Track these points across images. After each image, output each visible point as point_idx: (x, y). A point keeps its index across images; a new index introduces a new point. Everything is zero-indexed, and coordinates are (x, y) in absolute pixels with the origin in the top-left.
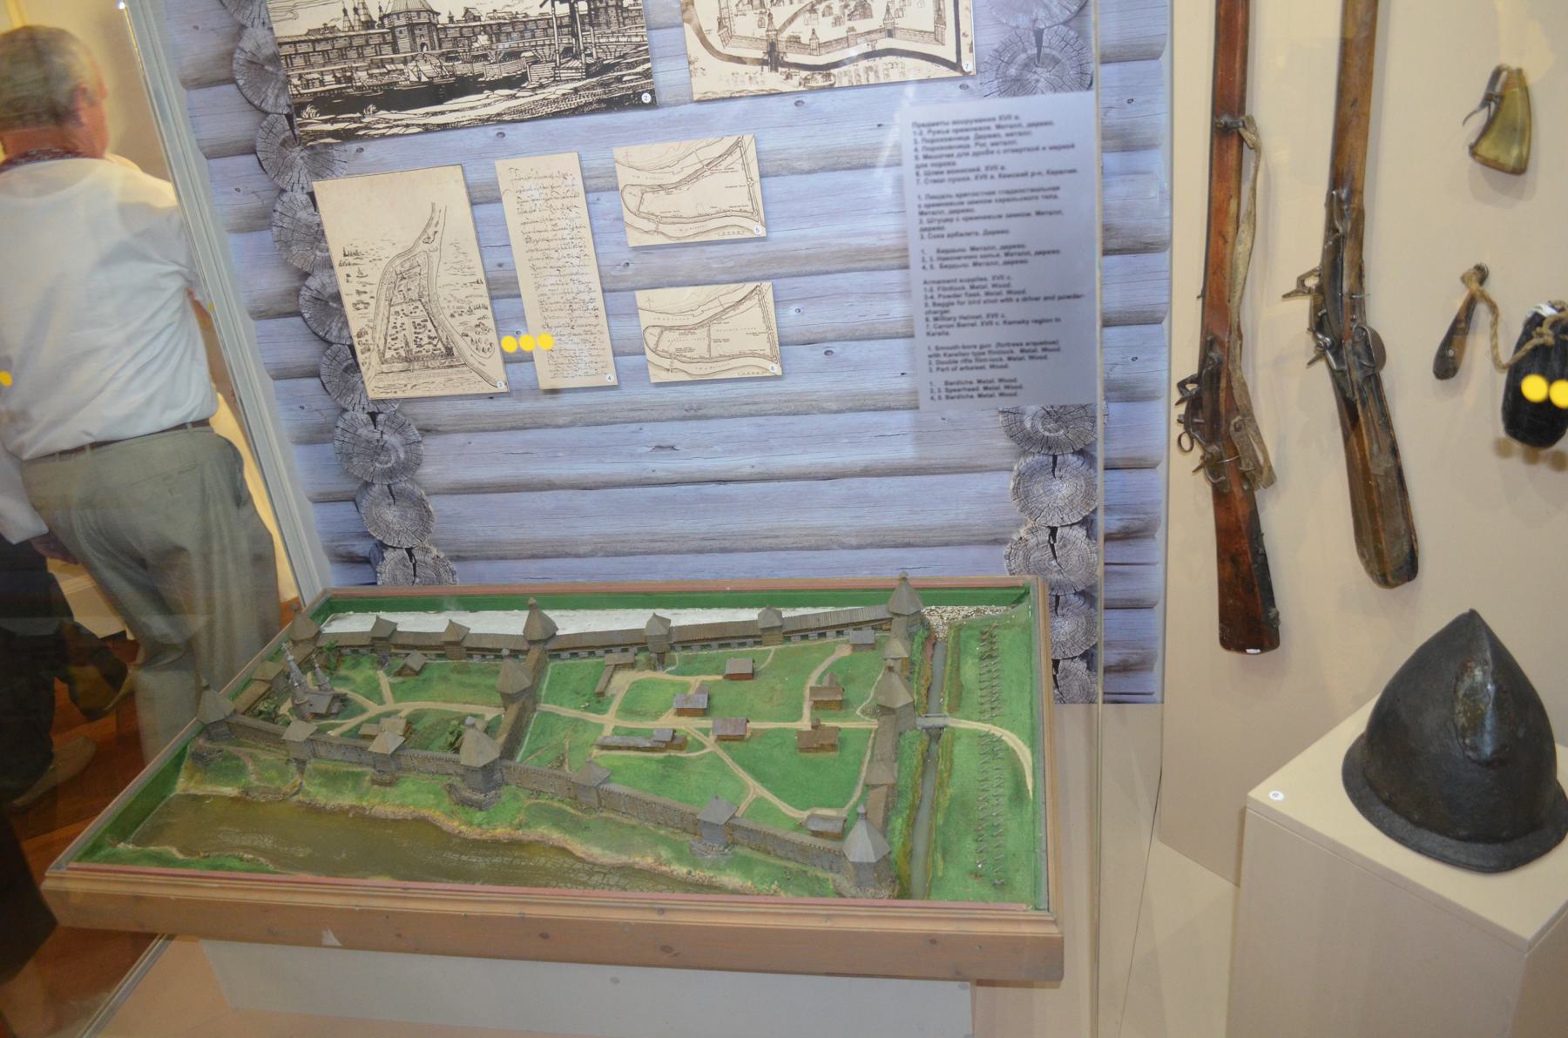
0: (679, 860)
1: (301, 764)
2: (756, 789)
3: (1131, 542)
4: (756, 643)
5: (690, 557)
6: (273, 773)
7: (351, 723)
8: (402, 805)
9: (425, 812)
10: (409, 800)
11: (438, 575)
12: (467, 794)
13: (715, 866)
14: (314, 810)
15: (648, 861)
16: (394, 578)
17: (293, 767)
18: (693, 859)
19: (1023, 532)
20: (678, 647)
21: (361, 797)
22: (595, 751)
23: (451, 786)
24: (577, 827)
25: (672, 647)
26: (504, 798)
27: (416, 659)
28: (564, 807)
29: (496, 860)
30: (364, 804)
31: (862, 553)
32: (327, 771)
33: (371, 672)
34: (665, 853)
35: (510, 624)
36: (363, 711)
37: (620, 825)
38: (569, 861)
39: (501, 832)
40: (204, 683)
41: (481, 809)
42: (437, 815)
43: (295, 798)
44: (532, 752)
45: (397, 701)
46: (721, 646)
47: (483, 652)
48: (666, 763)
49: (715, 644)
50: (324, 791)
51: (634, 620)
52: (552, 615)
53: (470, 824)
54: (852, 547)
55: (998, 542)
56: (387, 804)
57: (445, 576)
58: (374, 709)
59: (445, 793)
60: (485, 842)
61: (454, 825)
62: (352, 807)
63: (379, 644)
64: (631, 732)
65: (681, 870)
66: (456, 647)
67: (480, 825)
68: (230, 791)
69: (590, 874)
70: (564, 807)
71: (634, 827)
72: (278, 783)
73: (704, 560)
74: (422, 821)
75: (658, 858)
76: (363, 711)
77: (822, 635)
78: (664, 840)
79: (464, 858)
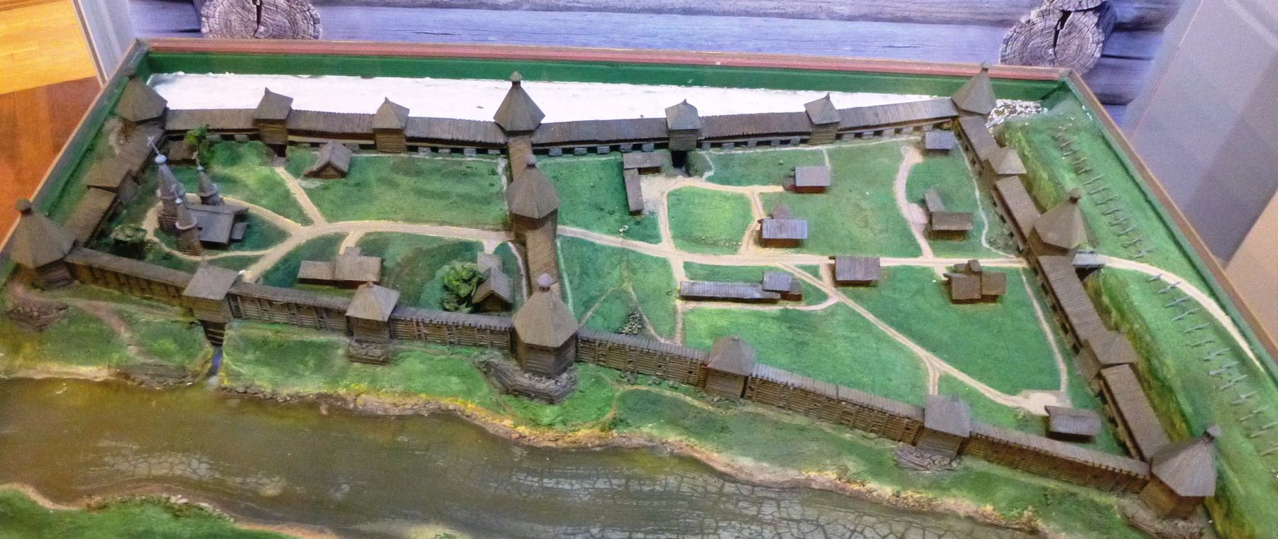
0: (876, 475)
1: (214, 333)
2: (935, 367)
3: (1139, 34)
4: (803, 142)
5: (642, 17)
6: (169, 345)
7: (272, 256)
8: (407, 393)
9: (450, 403)
10: (417, 384)
11: (294, 23)
12: (525, 380)
13: (936, 485)
14: (254, 401)
15: (827, 476)
16: (227, 25)
17: (199, 333)
18: (897, 472)
19: (1033, 15)
20: (706, 144)
21: (334, 381)
22: (679, 304)
23: (488, 364)
24: (707, 427)
25: (699, 145)
26: (582, 384)
27: (333, 152)
28: (681, 396)
29: (601, 484)
30: (342, 391)
31: (851, 26)
32: (265, 342)
33: (265, 171)
34: (853, 465)
35: (473, 102)
36: (282, 235)
37: (777, 425)
38: (701, 479)
39: (585, 433)
40: (238, 236)
41: (551, 401)
42: (471, 407)
43: (214, 381)
44: (587, 305)
45: (332, 218)
46: (759, 144)
47: (435, 144)
48: (785, 317)
49: (752, 141)
50: (265, 372)
51: (791, 102)
52: (533, 89)
53: (535, 423)
54: (842, 18)
55: (1004, 23)
56: (382, 391)
57: (302, 25)
58: (299, 234)
59: (480, 376)
60: (566, 451)
61: (505, 424)
62: (321, 396)
63: (266, 130)
64: (713, 273)
65: (886, 490)
66: (391, 137)
67: (550, 425)
68: (95, 371)
69: (759, 502)
70: (681, 396)
71: (802, 429)
72: (178, 359)
73: (659, 22)
74: (448, 417)
75: (843, 471)
76: (282, 235)
77: (878, 134)
78: (851, 448)
79: (549, 483)
